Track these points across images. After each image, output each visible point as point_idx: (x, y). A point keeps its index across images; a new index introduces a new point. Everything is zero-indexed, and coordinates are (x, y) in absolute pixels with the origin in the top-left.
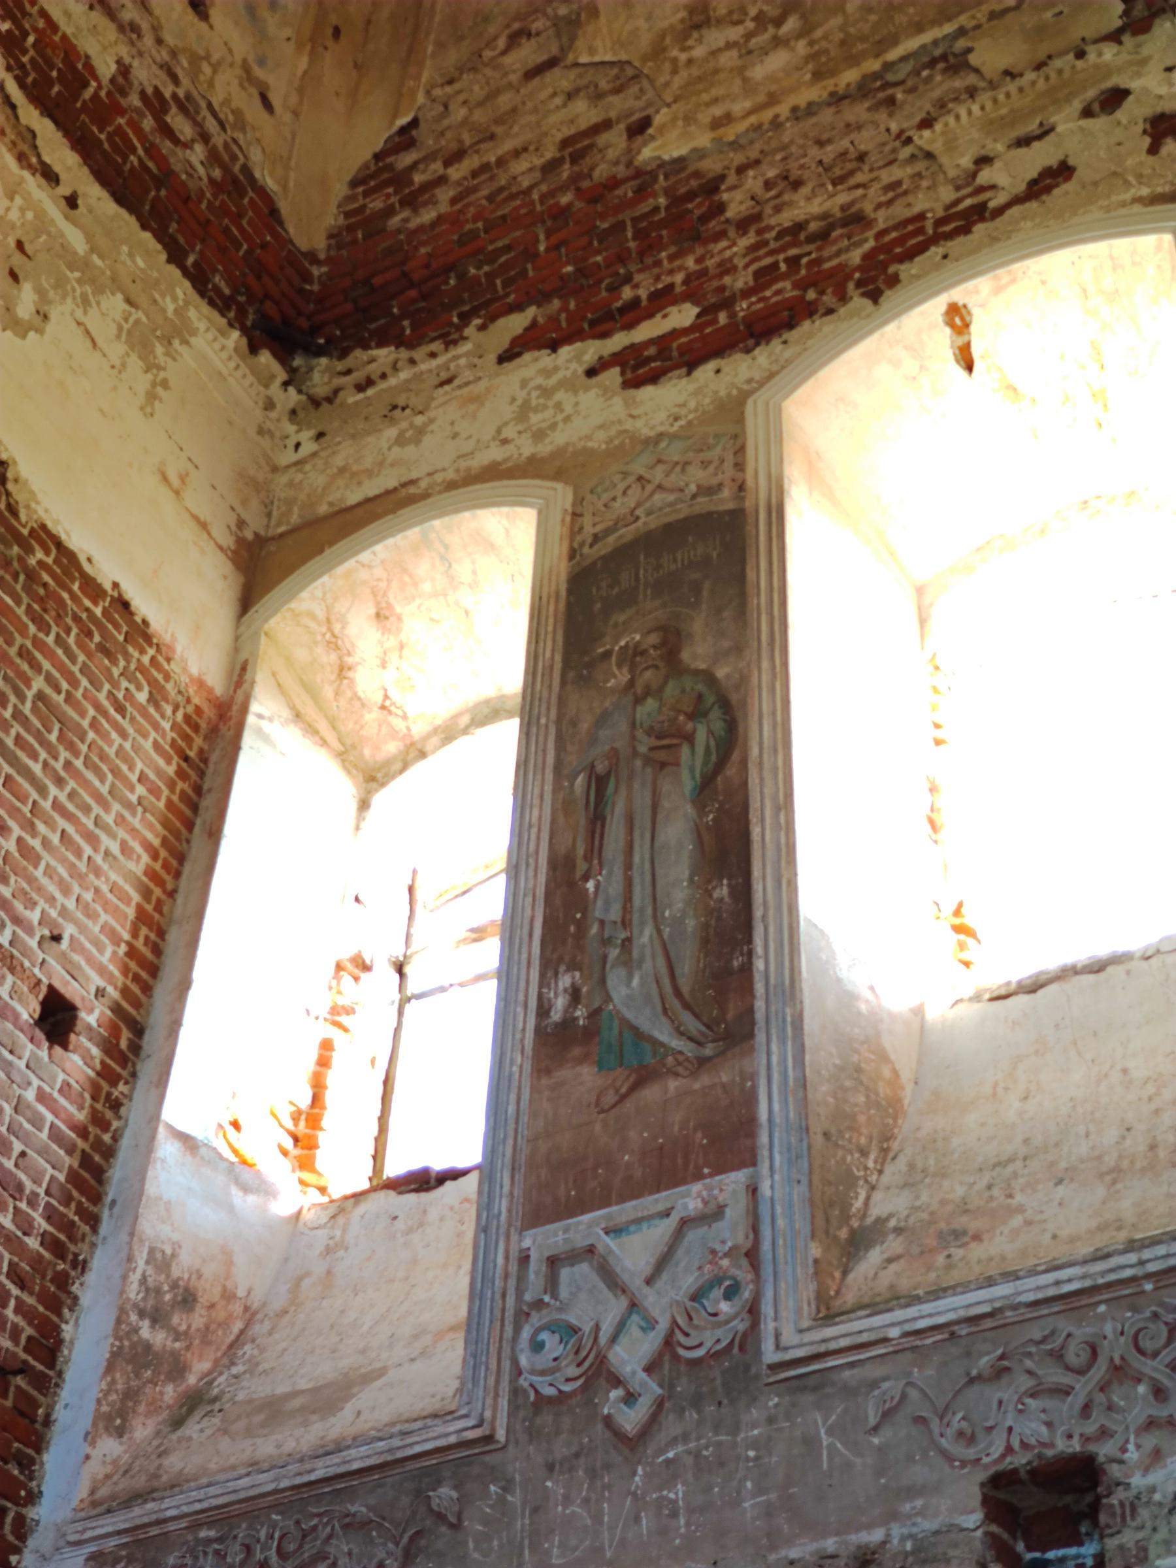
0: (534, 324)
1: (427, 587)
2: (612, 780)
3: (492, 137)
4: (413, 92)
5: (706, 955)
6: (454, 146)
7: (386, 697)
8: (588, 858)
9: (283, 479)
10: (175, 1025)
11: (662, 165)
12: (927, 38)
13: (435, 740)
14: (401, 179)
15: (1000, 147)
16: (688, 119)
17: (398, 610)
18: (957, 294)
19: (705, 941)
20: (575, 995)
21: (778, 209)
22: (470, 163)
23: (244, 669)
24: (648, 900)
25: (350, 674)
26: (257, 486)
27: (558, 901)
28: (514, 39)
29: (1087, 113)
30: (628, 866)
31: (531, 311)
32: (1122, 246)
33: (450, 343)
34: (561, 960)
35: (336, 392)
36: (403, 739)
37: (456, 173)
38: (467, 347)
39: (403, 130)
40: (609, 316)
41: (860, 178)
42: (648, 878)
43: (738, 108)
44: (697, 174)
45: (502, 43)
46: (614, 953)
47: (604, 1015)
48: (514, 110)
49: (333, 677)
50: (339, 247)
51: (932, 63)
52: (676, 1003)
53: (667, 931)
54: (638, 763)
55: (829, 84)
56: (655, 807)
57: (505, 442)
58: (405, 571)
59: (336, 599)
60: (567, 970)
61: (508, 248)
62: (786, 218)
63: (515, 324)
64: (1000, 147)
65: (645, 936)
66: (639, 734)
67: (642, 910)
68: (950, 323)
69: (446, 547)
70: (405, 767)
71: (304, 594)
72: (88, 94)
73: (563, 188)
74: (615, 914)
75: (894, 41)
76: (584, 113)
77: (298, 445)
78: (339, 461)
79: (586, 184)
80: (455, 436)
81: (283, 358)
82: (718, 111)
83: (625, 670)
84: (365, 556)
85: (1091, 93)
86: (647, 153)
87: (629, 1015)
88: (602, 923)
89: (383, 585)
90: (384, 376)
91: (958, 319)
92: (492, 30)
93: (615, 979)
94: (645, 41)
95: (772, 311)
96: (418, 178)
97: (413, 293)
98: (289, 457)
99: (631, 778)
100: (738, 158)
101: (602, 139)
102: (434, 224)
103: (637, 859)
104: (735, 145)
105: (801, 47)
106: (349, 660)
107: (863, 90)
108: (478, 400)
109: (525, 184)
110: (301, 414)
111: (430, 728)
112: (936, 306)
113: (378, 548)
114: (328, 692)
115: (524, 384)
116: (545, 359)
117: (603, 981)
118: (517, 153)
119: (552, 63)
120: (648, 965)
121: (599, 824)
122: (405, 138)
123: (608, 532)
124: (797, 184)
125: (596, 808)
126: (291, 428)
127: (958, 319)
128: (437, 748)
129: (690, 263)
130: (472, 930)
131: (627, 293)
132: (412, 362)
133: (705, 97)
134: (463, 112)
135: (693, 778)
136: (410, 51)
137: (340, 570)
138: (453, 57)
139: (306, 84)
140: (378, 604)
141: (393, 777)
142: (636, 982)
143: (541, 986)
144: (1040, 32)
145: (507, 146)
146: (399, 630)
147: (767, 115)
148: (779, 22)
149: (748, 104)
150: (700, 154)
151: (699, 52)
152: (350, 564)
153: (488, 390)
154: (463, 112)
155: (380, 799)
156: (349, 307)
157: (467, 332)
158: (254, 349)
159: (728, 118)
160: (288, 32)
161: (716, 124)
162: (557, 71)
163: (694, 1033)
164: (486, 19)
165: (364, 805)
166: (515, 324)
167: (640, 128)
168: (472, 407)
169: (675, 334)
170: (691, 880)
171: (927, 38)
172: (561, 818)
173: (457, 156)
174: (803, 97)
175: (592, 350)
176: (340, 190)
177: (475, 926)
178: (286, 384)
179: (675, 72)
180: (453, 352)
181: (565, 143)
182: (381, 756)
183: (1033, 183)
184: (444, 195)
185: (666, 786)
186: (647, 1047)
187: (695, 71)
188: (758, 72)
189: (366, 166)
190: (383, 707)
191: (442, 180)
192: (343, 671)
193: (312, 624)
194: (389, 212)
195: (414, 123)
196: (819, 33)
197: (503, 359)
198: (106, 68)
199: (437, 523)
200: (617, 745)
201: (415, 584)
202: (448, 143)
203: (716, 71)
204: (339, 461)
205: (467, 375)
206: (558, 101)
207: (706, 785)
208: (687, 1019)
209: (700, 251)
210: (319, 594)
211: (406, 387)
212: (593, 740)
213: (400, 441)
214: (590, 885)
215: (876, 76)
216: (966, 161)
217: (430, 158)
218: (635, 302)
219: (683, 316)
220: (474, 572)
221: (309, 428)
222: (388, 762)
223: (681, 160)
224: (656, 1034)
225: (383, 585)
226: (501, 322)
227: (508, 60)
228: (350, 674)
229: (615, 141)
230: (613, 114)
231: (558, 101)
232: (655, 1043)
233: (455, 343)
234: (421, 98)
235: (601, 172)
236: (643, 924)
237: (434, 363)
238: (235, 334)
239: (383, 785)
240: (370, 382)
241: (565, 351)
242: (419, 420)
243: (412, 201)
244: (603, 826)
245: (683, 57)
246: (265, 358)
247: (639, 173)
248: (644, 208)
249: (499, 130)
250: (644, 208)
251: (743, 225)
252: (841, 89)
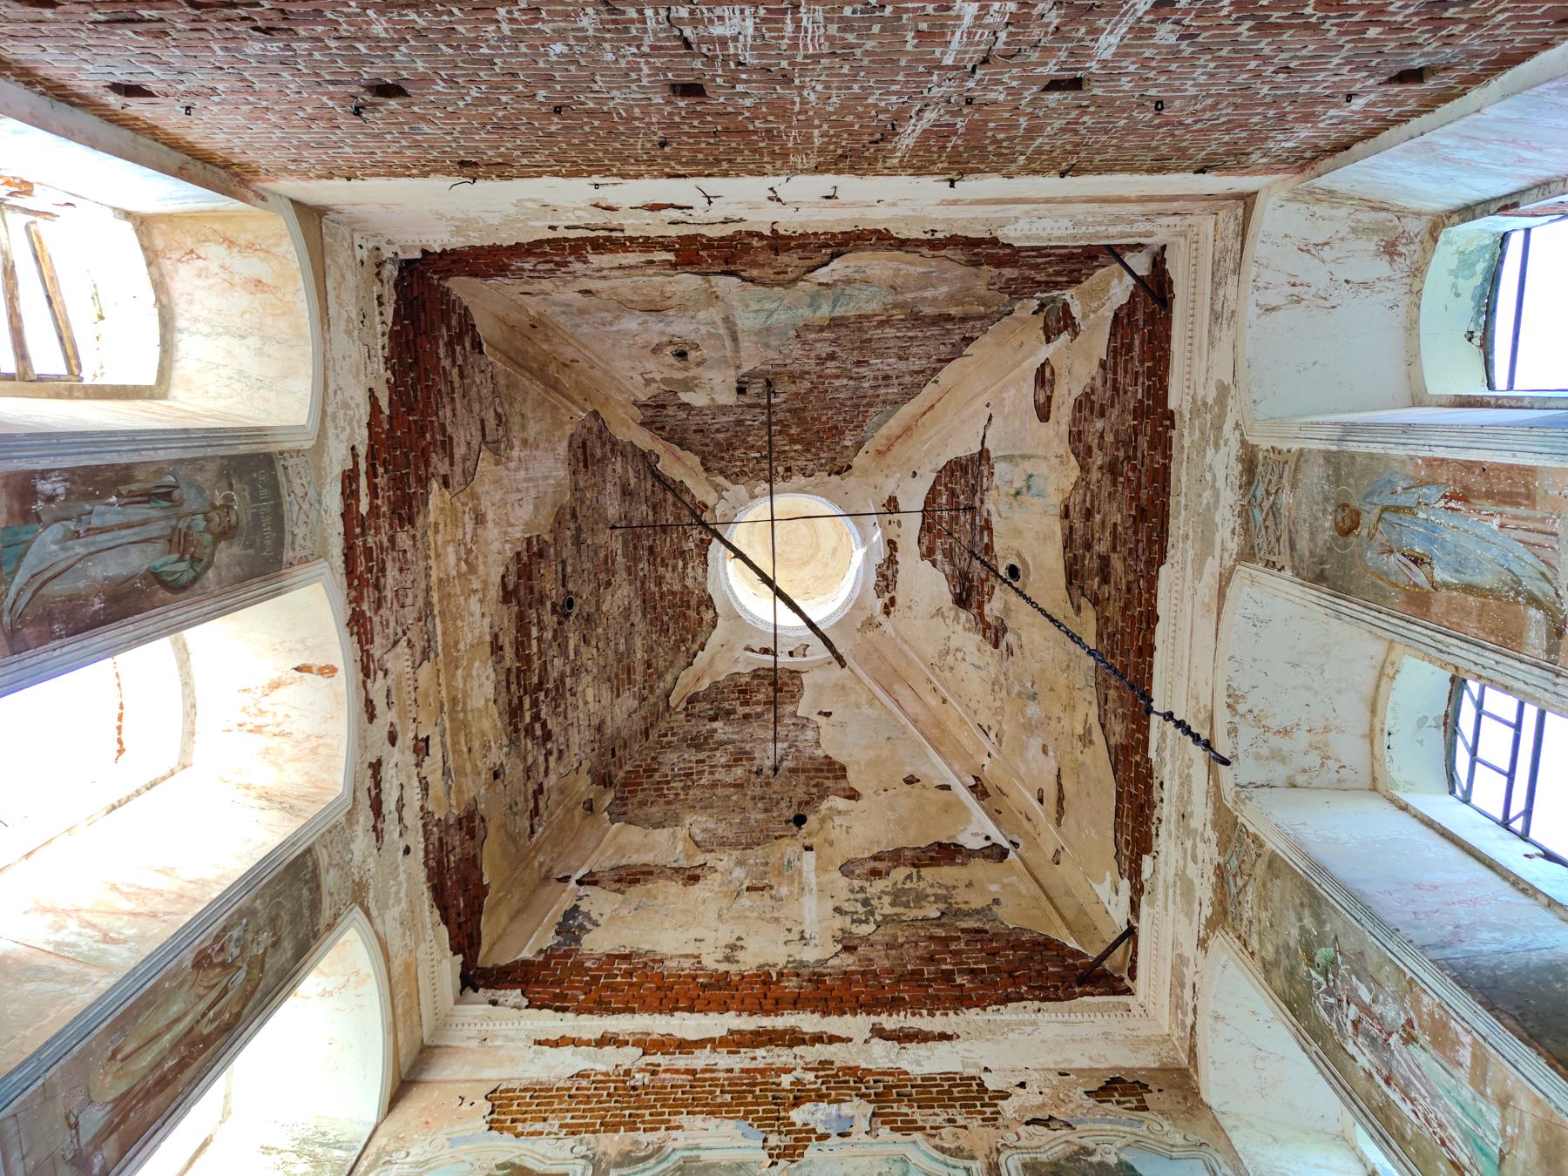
0: (382, 412)
1: (269, 321)
2: (168, 504)
3: (464, 396)
4: (494, 356)
5: (63, 602)
6: (466, 373)
7: (199, 257)
8: (131, 494)
9: (347, 234)
10: (68, 134)
11: (428, 493)
12: (439, 638)
13: (156, 274)
14: (460, 338)
15: (389, 682)
16: (442, 509)
17: (258, 296)
18: (341, 674)
19: (71, 599)
20: (51, 499)
21: (394, 560)
22: (456, 378)
23: (264, 199)
24: (100, 547)
25: (225, 245)
26: (350, 224)
27: (109, 474)
28: (498, 416)
29: (392, 725)
30: (122, 527)
31: (387, 412)
32: (341, 762)
33: (387, 360)
34: (74, 483)
35: (381, 281)
36: (163, 251)
37: (455, 371)
38: (382, 371)
39: (480, 345)
40: (374, 458)
41: (395, 604)
42: (111, 544)
43: (439, 537)
44: (418, 512)
45: (499, 410)
46: (72, 525)
47: (37, 526)
48: (471, 412)
49: (228, 235)
50: (442, 293)
51: (429, 641)
52: (37, 584)
53: (79, 566)
54: (174, 522)
55: (435, 588)
56: (148, 540)
57: (336, 393)
58: (284, 313)
59: (281, 263)
60: (67, 489)
61: (415, 398)
62: (389, 564)
63: (384, 404)
64: (389, 682)
65: (79, 549)
66: (189, 519)
67: (94, 543)
68: (326, 667)
69: (292, 347)
70: (144, 248)
71: (292, 248)
72: (589, 248)
73: (433, 436)
74: (96, 522)
75: (442, 622)
76: (460, 451)
77: (361, 247)
78: (349, 275)
79: (431, 449)
80: (344, 358)
81: (409, 262)
82: (441, 527)
83: (222, 502)
84: (302, 295)
85: (398, 728)
86: (435, 485)
87: (34, 547)
88: (91, 513)
89: (280, 296)
90: (381, 314)
91: (328, 671)
92: (506, 406)
93: (56, 530)
94: (479, 489)
95: (354, 562)
96: (458, 348)
97: (411, 336)
98: (357, 241)
99: (168, 518)
100: (419, 535)
101: (447, 460)
102: (437, 354)
103: (124, 532)
104: (425, 534)
105: (454, 573)
106: (236, 250)
107: (428, 604)
108: (356, 376)
109: (440, 413)
110: (375, 253)
111: (165, 272)
112: (339, 662)
113: (305, 305)
114: (218, 226)
115: (358, 405)
116: (365, 420)
117: (57, 520)
118: (454, 410)
119: (484, 436)
120: (62, 555)
121: (146, 499)
122: (477, 346)
123: (287, 476)
124: (401, 570)
125: (155, 494)
126: (370, 245)
127: (328, 671)
128: (150, 274)
129: (384, 509)
130: (13, 266)
131: (381, 470)
132: (383, 334)
133: (449, 520)
134: (478, 382)
135: (161, 566)
136: (511, 359)
137: (299, 276)
138: (502, 381)
139: (522, 309)
140: (268, 286)
141: (140, 239)
142: (54, 547)
143: (59, 469)
144: (426, 696)
145: (458, 405)
146: (244, 289)
147: (432, 553)
148: (466, 561)
149: (439, 543)
150: (426, 516)
151: (467, 517)
152: (301, 284)
153: (360, 382)
154: (478, 382)
155: (127, 227)
156: (415, 294)
157: (389, 372)
158: (425, 252)
159: (437, 532)
160: (549, 312)
161: (436, 525)
162: (480, 438)
163: (18, 604)
164: (511, 404)
165: (128, 215)
166: (384, 404)
167: (446, 483)
168: (354, 370)
169: (358, 500)
170: (106, 578)
171: (439, 638)
172: (153, 468)
173: (462, 376)
174: (434, 573)
175: (362, 450)
176: (466, 302)
177: (16, 269)
178: (396, 254)
179: (463, 504)
180: (382, 360)
181: (451, 439)
182: (156, 233)
183: (371, 701)
184: (446, 363)
185: (159, 546)
186: (12, 567)
187: (460, 515)
188: (451, 549)
189: (472, 319)
190: (192, 251)
191: (454, 363)
192: (231, 243)
193: (271, 242)
194: (449, 328)
195: (481, 352)
196: (456, 582)
197: (371, 390)
198: (591, 258)
199: (310, 349)
200: (186, 504)
201: (273, 315)
202: (468, 370)
203: (457, 526)
204: (349, 275)
205: (369, 369)
206: (468, 438)
207: (155, 577)
208: (28, 595)
209: (388, 515)
210: (289, 256)
211: (372, 327)
212: (190, 484)
213: (349, 319)
214: (114, 499)
215: (432, 611)
216: (389, 665)
217: (465, 360)
218: (375, 476)
219: (364, 508)
220: (269, 356)
221: (369, 257)
222: (149, 235)
223: (427, 505)
224: (20, 572)
225: (280, 296)
226: (387, 392)
227: (492, 411)
228: (225, 245)
229: (442, 467)
230: (455, 468)
231: (468, 438)
232: (14, 572)
233: (386, 363)
234: (490, 359)
235: (434, 458)
236: (86, 545)
237: (380, 347)
238: (438, 251)
239: (137, 230)
240: (381, 304)
241: (365, 432)
242: (356, 333)
243: (450, 344)
244: (144, 502)
245: (467, 509)
246: (418, 255)
247: (428, 479)
248: (412, 480)
249: (466, 401)
250: (412, 480)
251: (392, 540)
252: (432, 593)
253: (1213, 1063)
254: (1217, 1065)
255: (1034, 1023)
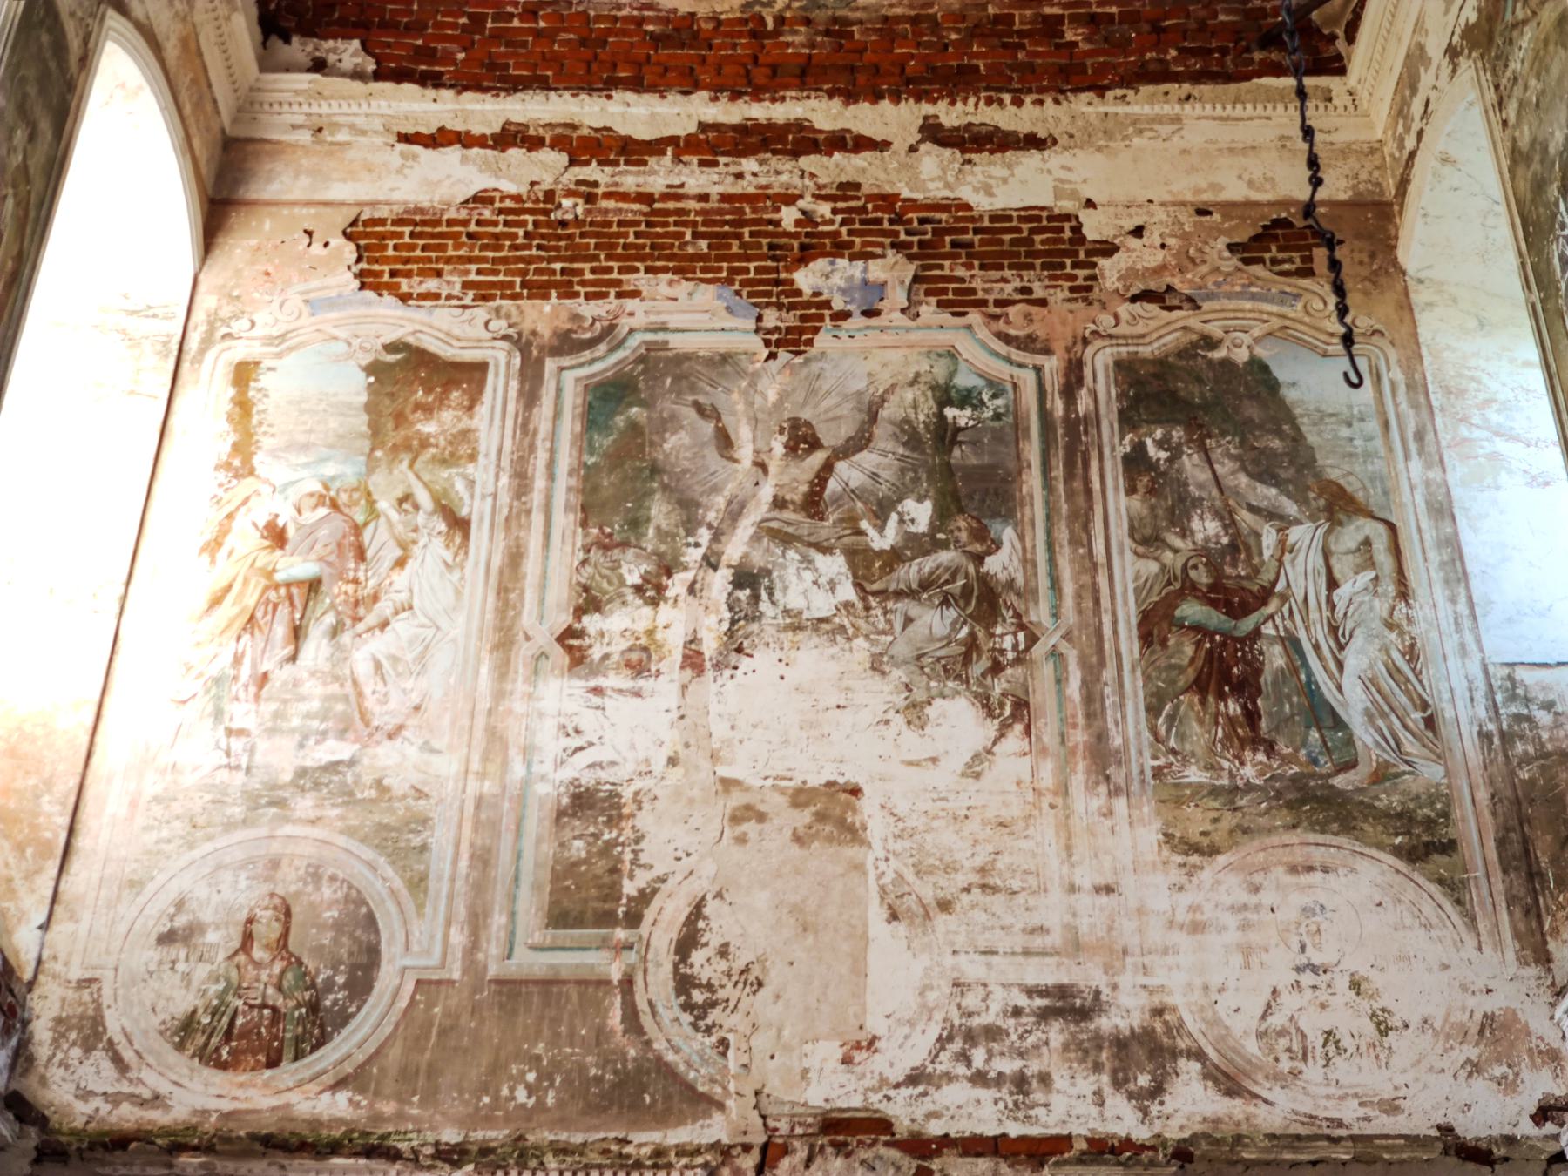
253: (1425, 215)
254: (1429, 220)
255: (1177, 120)
